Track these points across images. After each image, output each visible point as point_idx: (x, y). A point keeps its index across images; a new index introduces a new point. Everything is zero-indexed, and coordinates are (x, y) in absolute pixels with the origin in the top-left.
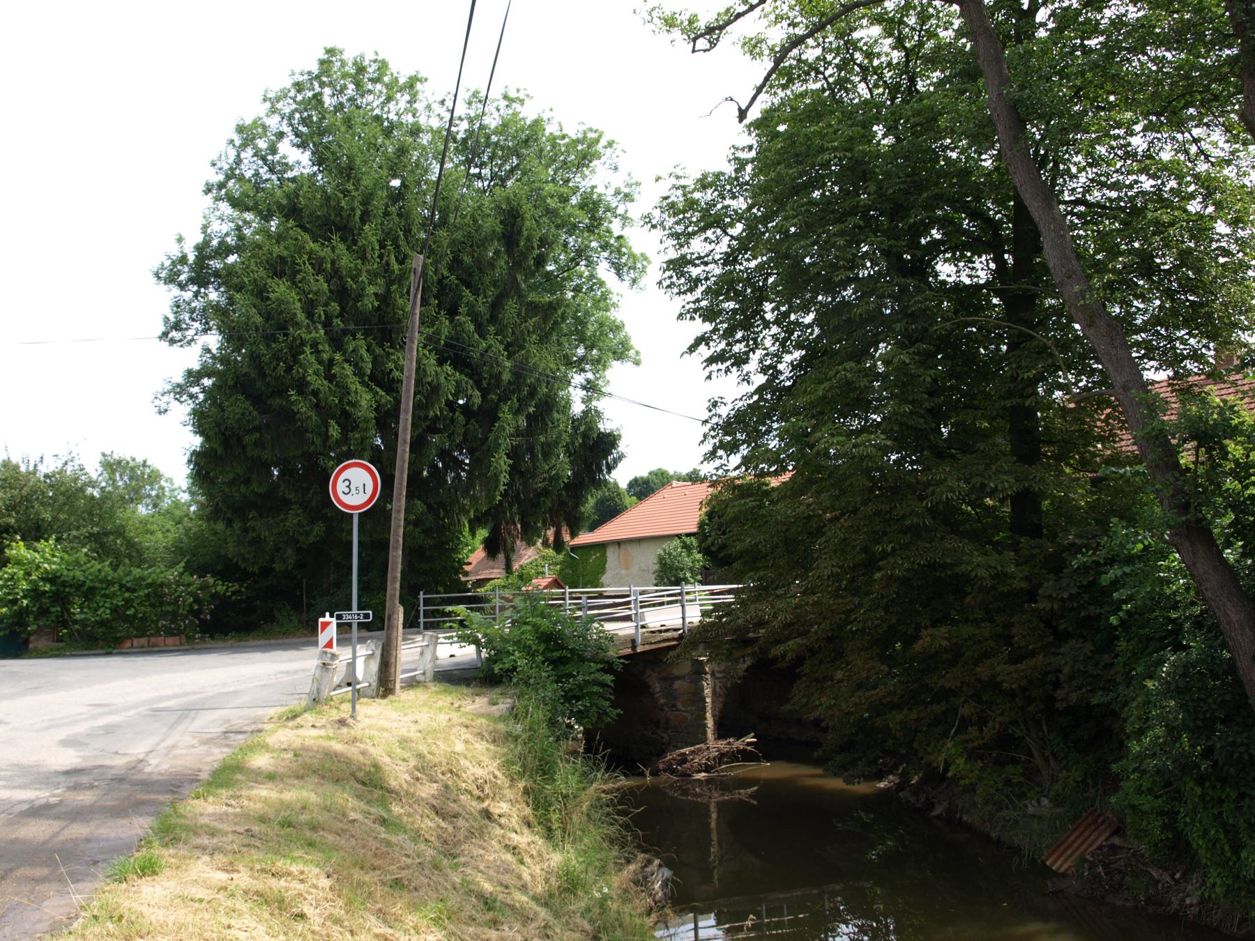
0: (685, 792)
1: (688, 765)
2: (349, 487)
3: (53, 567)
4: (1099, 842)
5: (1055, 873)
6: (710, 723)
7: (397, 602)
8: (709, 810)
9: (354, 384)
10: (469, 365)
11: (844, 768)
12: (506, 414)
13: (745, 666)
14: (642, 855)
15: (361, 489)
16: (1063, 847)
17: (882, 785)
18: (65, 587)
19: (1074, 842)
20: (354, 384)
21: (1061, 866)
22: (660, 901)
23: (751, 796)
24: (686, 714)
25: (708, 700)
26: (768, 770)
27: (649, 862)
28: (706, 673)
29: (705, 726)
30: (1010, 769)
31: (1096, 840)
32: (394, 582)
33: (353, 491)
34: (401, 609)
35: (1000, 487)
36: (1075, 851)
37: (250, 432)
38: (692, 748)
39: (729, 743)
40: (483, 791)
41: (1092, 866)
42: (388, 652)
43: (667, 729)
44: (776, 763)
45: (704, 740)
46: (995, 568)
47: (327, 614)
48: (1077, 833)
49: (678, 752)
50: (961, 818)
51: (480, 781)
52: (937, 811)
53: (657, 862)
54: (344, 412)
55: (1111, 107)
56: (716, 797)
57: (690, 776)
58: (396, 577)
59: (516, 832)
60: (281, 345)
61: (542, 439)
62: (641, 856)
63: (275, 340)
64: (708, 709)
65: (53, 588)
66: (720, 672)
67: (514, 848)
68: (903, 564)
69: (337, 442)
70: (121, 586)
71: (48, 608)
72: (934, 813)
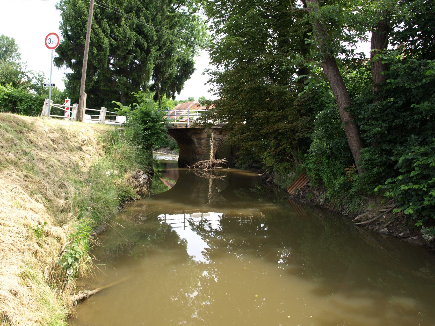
0: (201, 174)
2: (50, 41)
3: (9, 91)
6: (212, 154)
7: (84, 91)
8: (209, 180)
9: (103, 35)
10: (144, 34)
12: (153, 49)
15: (54, 42)
16: (293, 186)
18: (13, 98)
20: (103, 35)
26: (229, 170)
28: (212, 138)
29: (210, 155)
33: (52, 43)
34: (86, 95)
35: (283, 61)
37: (69, 50)
39: (217, 161)
43: (198, 155)
46: (280, 90)
47: (68, 98)
48: (298, 181)
49: (200, 162)
51: (83, 140)
53: (142, 172)
54: (99, 45)
55: (429, 13)
56: (211, 177)
60: (79, 21)
63: (78, 20)
65: (9, 98)
67: (83, 158)
68: (248, 86)
69: (97, 55)
70: (31, 100)
71: (8, 104)
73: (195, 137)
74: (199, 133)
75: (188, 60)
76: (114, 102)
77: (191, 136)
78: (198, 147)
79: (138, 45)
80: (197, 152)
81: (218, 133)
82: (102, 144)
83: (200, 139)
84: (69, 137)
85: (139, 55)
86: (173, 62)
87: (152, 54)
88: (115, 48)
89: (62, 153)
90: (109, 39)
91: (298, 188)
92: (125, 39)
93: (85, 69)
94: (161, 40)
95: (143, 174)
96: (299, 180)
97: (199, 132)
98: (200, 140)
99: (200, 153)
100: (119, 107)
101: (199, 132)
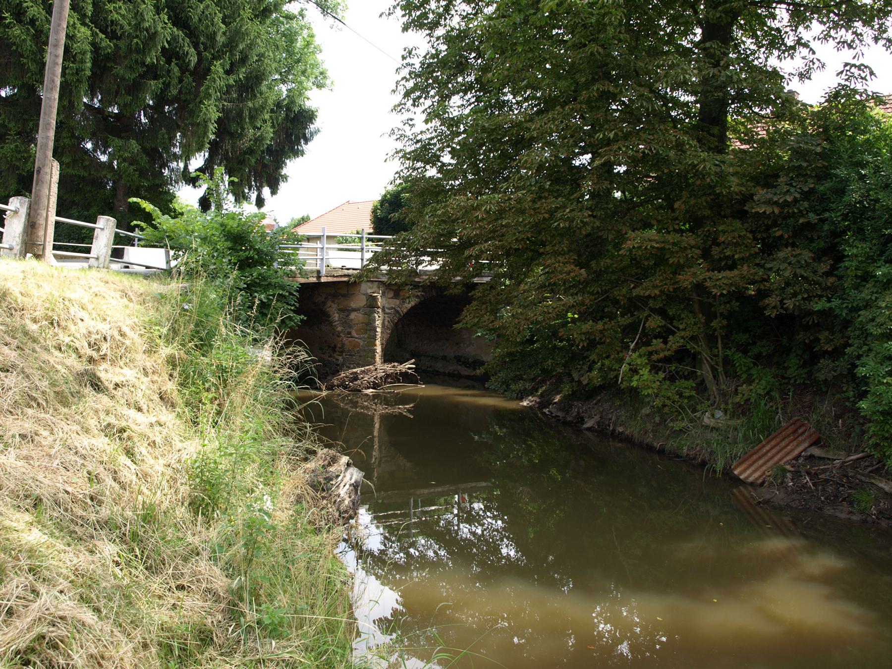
0: (355, 404)
1: (359, 382)
4: (796, 452)
5: (743, 482)
6: (379, 349)
7: (50, 153)
11: (506, 384)
12: (218, 67)
13: (410, 306)
14: (325, 450)
16: (755, 457)
17: (525, 403)
19: (768, 451)
21: (750, 475)
22: (346, 512)
23: (409, 411)
24: (359, 341)
25: (379, 330)
26: (422, 389)
27: (334, 460)
28: (378, 307)
29: (374, 351)
30: (683, 383)
31: (792, 450)
32: (47, 129)
34: (56, 166)
36: (768, 461)
38: (363, 369)
39: (394, 367)
40: (98, 350)
41: (797, 475)
42: (36, 211)
43: (342, 352)
44: (429, 385)
45: (373, 363)
49: (351, 371)
50: (614, 430)
51: (94, 337)
52: (589, 424)
58: (49, 124)
59: (139, 409)
61: (250, 104)
62: (322, 452)
64: (378, 337)
66: (389, 309)
67: (122, 430)
72: (586, 426)
73: (335, 306)
74: (344, 296)
75: (300, 106)
76: (135, 199)
77: (324, 303)
79: (171, 54)
80: (339, 346)
81: (391, 294)
82: (166, 351)
83: (346, 311)
84: (33, 327)
85: (175, 81)
86: (263, 108)
87: (215, 81)
88: (108, 57)
89: (28, 426)
90: (91, 30)
91: (782, 463)
92: (138, 33)
93: (54, 74)
94: (237, 46)
95: (346, 470)
96: (778, 440)
97: (344, 291)
98: (346, 314)
100: (148, 218)
101: (344, 291)
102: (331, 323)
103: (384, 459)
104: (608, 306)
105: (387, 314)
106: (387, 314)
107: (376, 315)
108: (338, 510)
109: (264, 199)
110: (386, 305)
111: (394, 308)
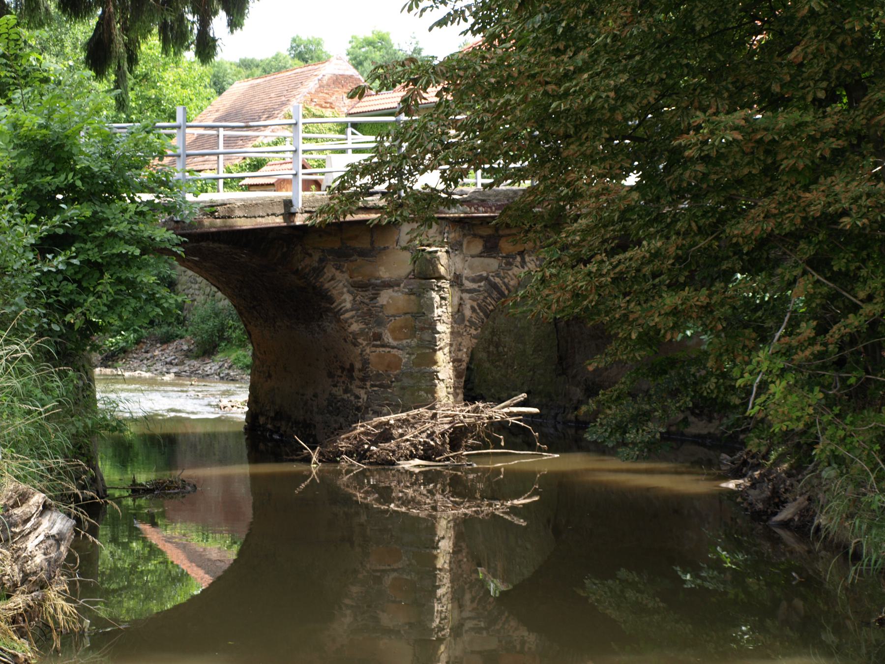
0: (385, 495)
28: (440, 278)
29: (433, 376)
38: (403, 415)
39: (476, 410)
43: (364, 380)
44: (564, 455)
45: (428, 398)
49: (376, 420)
52: (785, 514)
57: (393, 463)
66: (473, 280)
73: (342, 278)
74: (363, 254)
77: (319, 271)
78: (362, 332)
80: (358, 365)
81: (478, 247)
95: (42, 514)
98: (370, 293)
99: (373, 369)
101: (364, 243)
102: (337, 314)
103: (469, 625)
104: (728, 258)
105: (469, 291)
106: (469, 291)
107: (434, 294)
108: (22, 570)
109: (214, 40)
110: (466, 272)
111: (486, 279)
